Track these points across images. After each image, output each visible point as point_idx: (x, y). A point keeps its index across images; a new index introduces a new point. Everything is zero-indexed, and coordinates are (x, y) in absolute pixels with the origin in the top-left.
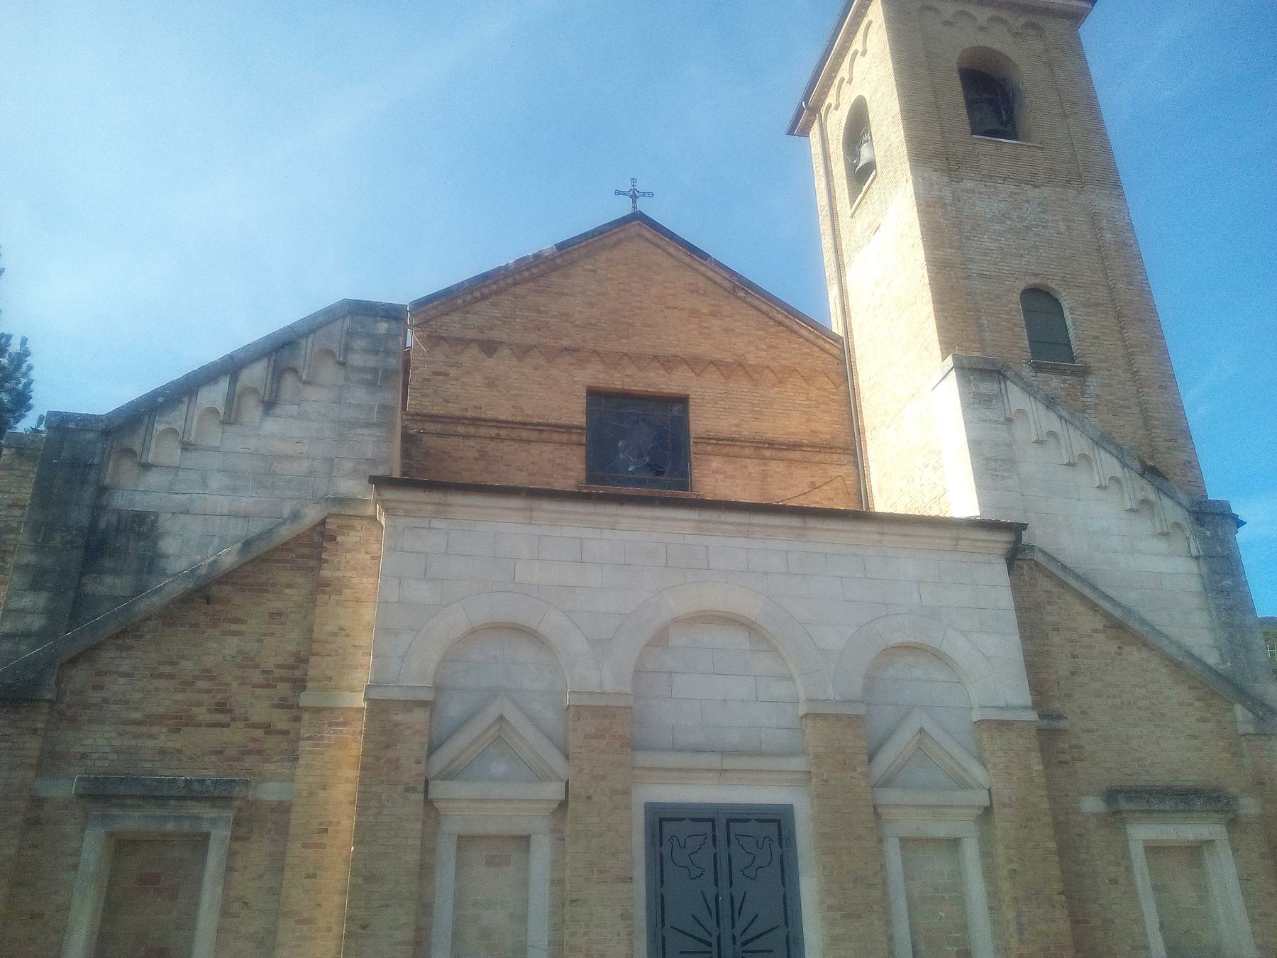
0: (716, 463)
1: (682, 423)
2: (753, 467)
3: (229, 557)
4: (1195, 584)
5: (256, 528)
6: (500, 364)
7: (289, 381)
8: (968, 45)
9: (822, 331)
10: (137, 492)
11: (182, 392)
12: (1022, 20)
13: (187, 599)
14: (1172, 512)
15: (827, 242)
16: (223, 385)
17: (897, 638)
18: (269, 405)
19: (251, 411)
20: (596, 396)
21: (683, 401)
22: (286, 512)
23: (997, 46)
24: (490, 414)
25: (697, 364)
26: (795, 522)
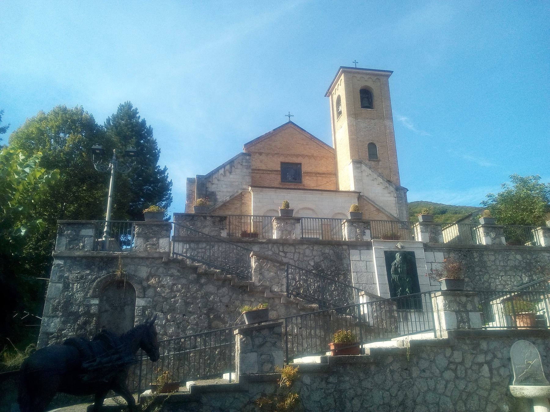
0: (307, 178)
1: (300, 169)
2: (315, 178)
3: (228, 199)
4: (394, 202)
5: (231, 194)
6: (263, 157)
7: (233, 168)
9: (332, 148)
10: (212, 188)
11: (217, 170)
13: (222, 206)
14: (392, 189)
16: (223, 169)
17: (337, 212)
18: (230, 173)
19: (228, 174)
20: (283, 164)
21: (300, 164)
22: (236, 191)
24: (261, 168)
25: (304, 156)
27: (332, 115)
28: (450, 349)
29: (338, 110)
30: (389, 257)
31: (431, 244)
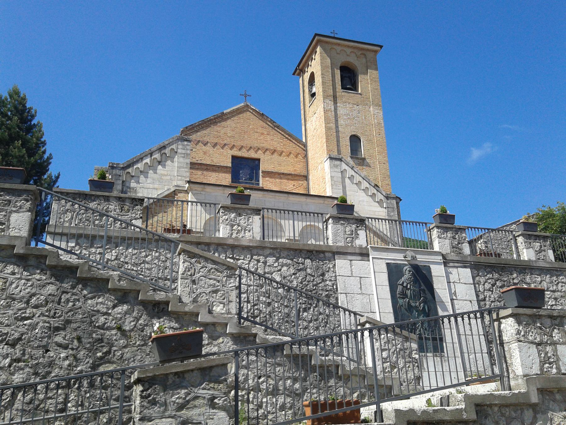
6: (208, 148)
8: (343, 61)
12: (360, 52)
15: (302, 112)
20: (234, 158)
21: (259, 160)
23: (352, 61)
24: (204, 162)
26: (286, 195)
27: (302, 99)
28: (531, 411)
29: (310, 91)
30: (394, 271)
31: (453, 256)
